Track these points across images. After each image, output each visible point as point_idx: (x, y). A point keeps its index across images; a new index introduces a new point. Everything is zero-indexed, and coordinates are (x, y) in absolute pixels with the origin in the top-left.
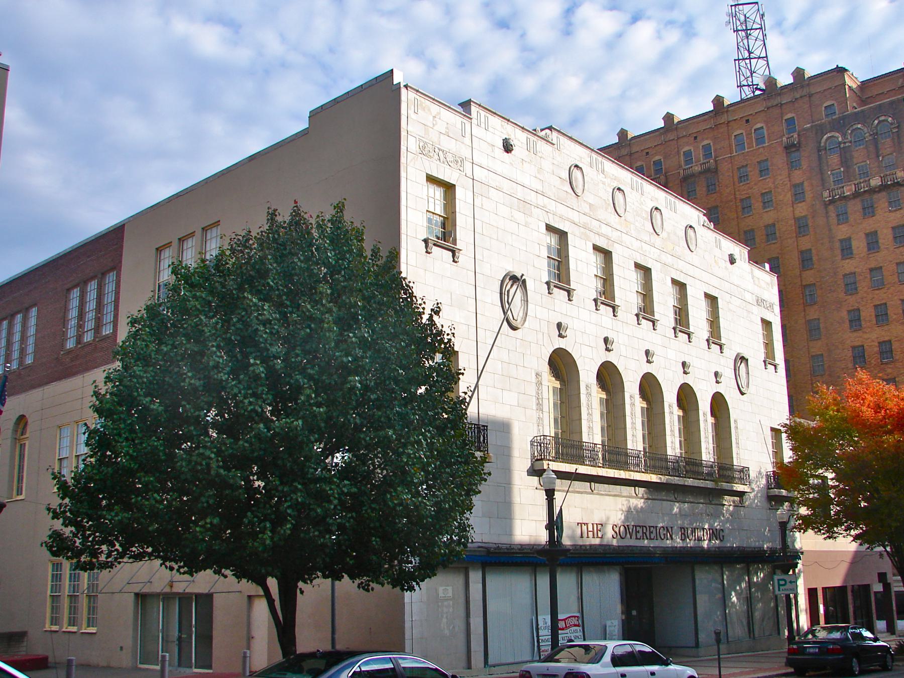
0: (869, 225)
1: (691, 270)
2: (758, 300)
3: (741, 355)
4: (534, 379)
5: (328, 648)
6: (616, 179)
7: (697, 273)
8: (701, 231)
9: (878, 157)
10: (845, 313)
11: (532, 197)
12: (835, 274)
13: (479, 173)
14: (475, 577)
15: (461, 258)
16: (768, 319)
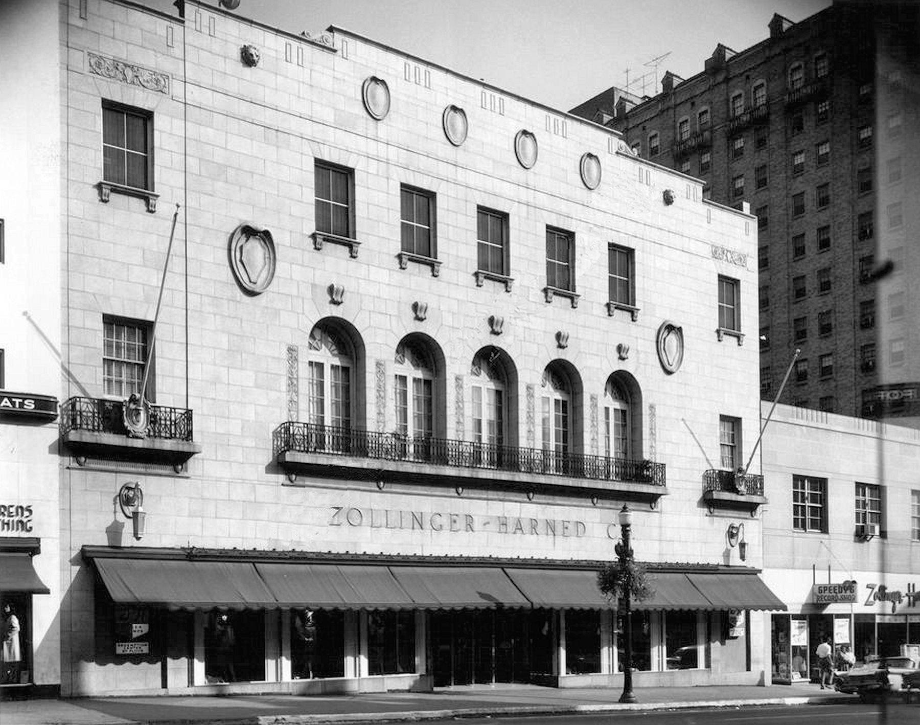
2: (716, 252)
3: (668, 323)
8: (609, 161)
13: (195, 95)
15: (745, 340)
16: (733, 276)
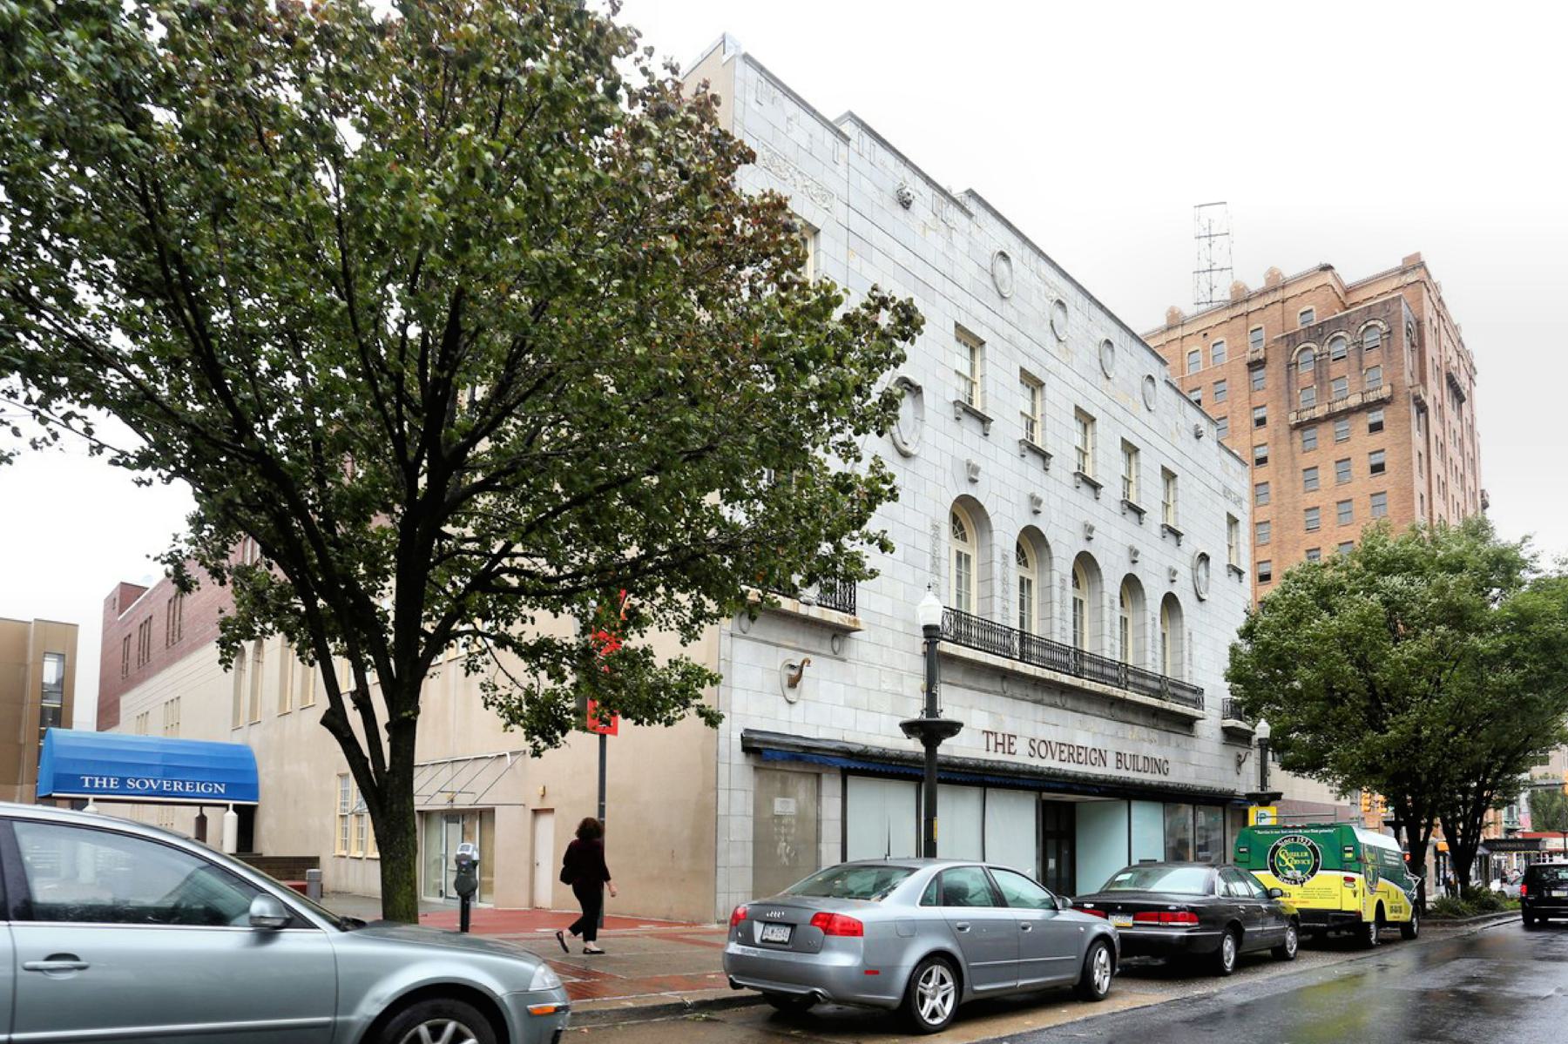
0: (1343, 451)
1: (1147, 435)
4: (929, 531)
5: (378, 863)
6: (1055, 289)
7: (1154, 439)
9: (1361, 369)
10: (1303, 553)
11: (935, 279)
12: (1295, 508)
14: (831, 786)
